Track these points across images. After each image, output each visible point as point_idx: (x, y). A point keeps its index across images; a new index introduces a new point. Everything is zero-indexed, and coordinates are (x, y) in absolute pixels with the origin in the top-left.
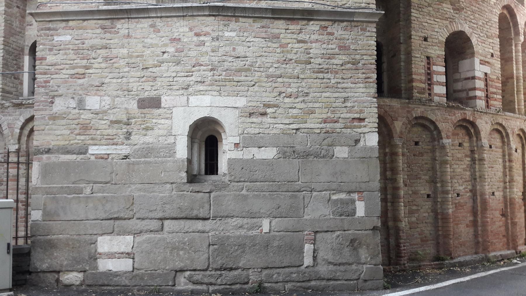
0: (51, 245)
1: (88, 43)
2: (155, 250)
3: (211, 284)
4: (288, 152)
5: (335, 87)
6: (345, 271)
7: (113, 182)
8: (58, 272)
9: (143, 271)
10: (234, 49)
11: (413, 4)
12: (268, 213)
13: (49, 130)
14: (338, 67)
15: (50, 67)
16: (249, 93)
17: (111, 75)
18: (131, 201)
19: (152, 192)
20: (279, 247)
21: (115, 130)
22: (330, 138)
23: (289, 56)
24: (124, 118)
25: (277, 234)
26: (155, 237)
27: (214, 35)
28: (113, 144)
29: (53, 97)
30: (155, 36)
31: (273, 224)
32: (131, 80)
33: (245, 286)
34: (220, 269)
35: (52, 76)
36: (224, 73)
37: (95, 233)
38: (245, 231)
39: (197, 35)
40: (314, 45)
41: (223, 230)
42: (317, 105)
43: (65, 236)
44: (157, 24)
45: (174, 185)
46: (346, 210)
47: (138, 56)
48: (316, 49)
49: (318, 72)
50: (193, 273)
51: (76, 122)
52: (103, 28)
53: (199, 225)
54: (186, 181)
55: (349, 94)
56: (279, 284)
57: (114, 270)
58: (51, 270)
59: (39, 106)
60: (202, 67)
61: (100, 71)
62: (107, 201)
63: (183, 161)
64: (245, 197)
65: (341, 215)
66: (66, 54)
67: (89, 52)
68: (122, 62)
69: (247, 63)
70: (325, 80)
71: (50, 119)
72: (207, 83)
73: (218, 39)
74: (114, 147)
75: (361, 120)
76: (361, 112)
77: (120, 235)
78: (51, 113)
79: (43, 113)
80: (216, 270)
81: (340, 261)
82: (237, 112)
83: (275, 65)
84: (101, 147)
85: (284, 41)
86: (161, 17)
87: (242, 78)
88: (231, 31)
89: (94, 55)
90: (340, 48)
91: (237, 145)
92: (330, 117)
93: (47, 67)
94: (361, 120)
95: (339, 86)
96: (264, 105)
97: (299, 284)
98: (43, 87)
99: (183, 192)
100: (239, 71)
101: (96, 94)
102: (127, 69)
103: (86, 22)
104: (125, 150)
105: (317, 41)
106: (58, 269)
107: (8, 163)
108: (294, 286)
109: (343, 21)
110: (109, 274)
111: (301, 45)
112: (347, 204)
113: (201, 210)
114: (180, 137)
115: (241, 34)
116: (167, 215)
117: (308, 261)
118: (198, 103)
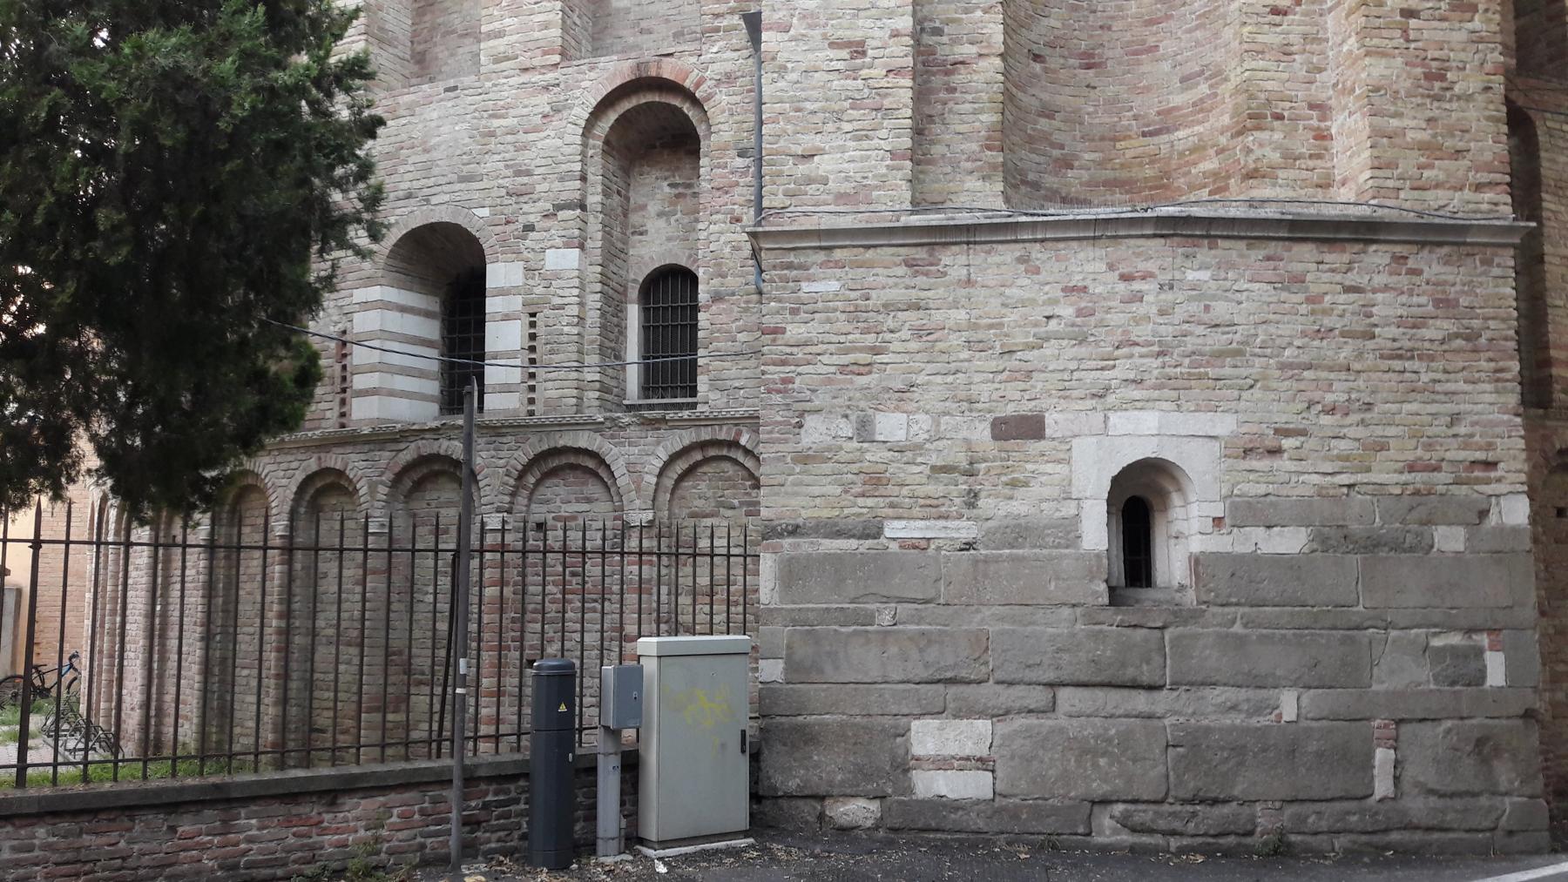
0: (806, 737)
1: (877, 298)
2: (1041, 753)
3: (1173, 833)
4: (1334, 539)
5: (1429, 392)
6: (1466, 810)
7: (942, 601)
8: (822, 798)
9: (1017, 800)
10: (1207, 308)
11: (1544, 181)
12: (1294, 677)
13: (794, 484)
14: (1435, 346)
15: (795, 350)
16: (1242, 405)
17: (930, 368)
18: (981, 643)
19: (1030, 623)
20: (1320, 754)
21: (941, 488)
22: (1424, 507)
23: (1328, 322)
24: (962, 460)
25: (1314, 724)
26: (1041, 725)
27: (1165, 277)
28: (939, 518)
29: (802, 414)
30: (1027, 282)
31: (1305, 701)
32: (977, 378)
33: (1248, 840)
34: (1191, 802)
35: (800, 369)
36: (1187, 361)
37: (906, 711)
38: (1243, 716)
39: (1125, 278)
40: (1380, 296)
41: (1194, 713)
42: (1391, 431)
43: (838, 717)
44: (1033, 256)
45: (1079, 610)
46: (1463, 670)
47: (991, 326)
48: (1385, 307)
49: (1391, 357)
50: (1131, 807)
51: (854, 468)
52: (909, 264)
53: (1140, 701)
54: (1106, 601)
55: (1462, 407)
56: (1320, 837)
57: (952, 796)
58: (806, 792)
59: (771, 432)
60: (1137, 350)
61: (906, 358)
62: (929, 641)
63: (1098, 556)
64: (1241, 640)
65: (1453, 683)
66: (829, 321)
67: (880, 318)
68: (955, 340)
69: (1237, 337)
70: (1407, 375)
71: (795, 461)
72: (1148, 383)
73: (1171, 288)
74: (942, 523)
75: (1490, 465)
76: (1490, 447)
77: (961, 718)
78: (799, 447)
79: (781, 447)
80: (1184, 802)
81: (1453, 788)
82: (1216, 446)
83: (1297, 343)
84: (913, 524)
85: (1314, 289)
86: (1042, 241)
87: (1227, 371)
88: (1198, 269)
89: (890, 323)
90: (1437, 303)
91: (1218, 521)
92: (1420, 459)
93: (788, 350)
94: (1490, 465)
95: (1438, 387)
96: (1277, 431)
97: (1364, 838)
98: (779, 391)
99: (1097, 627)
100: (1220, 355)
101: (897, 409)
102: (965, 355)
103: (871, 251)
104: (965, 530)
105: (1386, 288)
106: (822, 792)
107: (622, 554)
108: (1355, 842)
109: (1440, 244)
110: (940, 805)
111: (1353, 297)
112: (1466, 657)
113: (1145, 667)
114: (1089, 502)
115: (1223, 275)
116: (1065, 676)
117: (1382, 786)
118: (1130, 428)
